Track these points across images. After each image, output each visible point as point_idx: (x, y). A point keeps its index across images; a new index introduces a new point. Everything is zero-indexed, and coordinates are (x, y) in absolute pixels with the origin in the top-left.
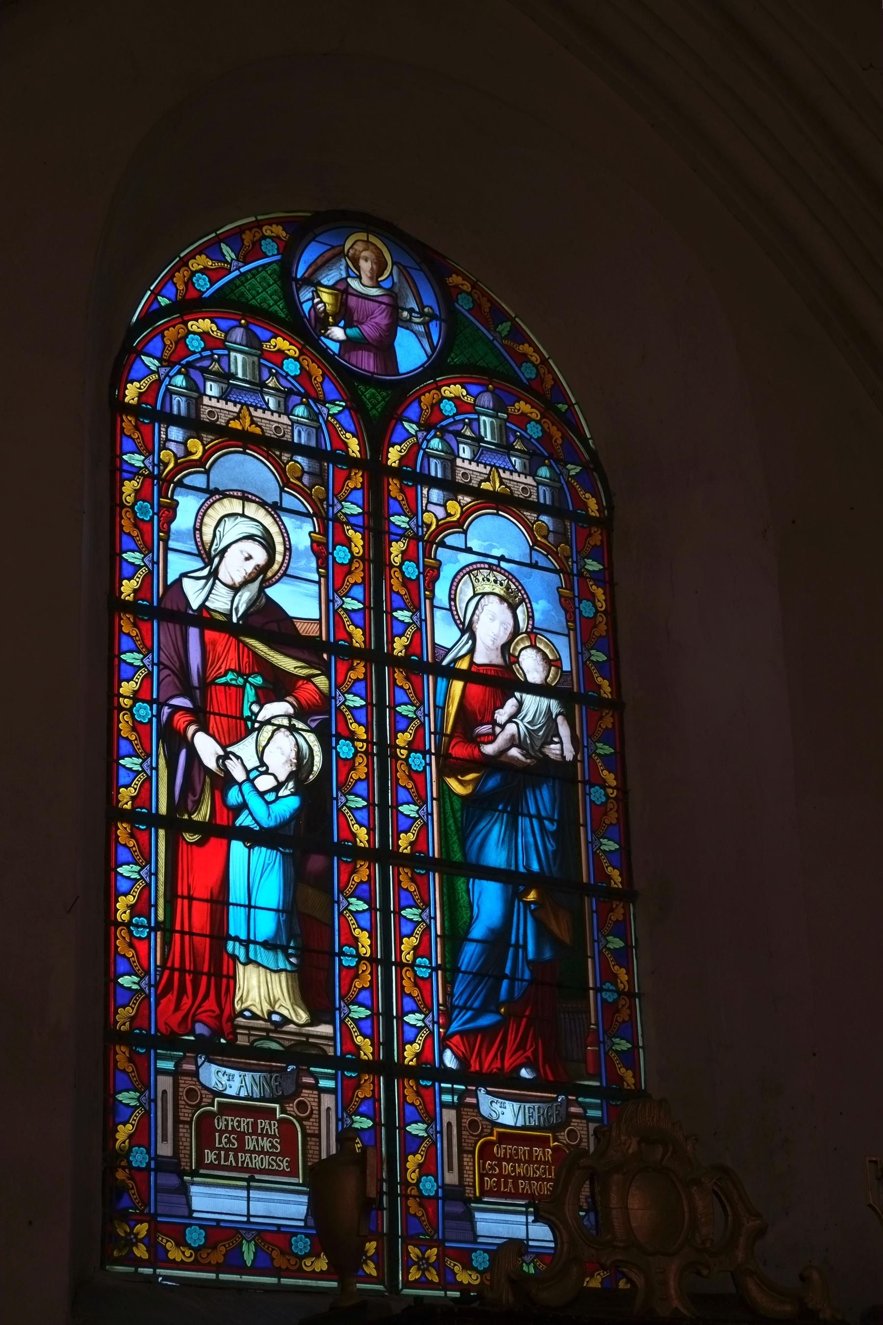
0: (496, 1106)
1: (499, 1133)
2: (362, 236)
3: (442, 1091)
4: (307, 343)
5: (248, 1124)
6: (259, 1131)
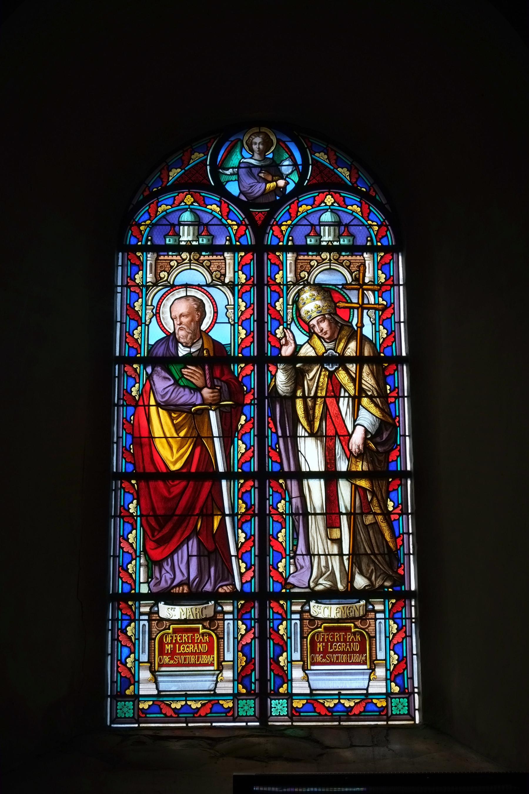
5: (188, 637)
6: (348, 640)
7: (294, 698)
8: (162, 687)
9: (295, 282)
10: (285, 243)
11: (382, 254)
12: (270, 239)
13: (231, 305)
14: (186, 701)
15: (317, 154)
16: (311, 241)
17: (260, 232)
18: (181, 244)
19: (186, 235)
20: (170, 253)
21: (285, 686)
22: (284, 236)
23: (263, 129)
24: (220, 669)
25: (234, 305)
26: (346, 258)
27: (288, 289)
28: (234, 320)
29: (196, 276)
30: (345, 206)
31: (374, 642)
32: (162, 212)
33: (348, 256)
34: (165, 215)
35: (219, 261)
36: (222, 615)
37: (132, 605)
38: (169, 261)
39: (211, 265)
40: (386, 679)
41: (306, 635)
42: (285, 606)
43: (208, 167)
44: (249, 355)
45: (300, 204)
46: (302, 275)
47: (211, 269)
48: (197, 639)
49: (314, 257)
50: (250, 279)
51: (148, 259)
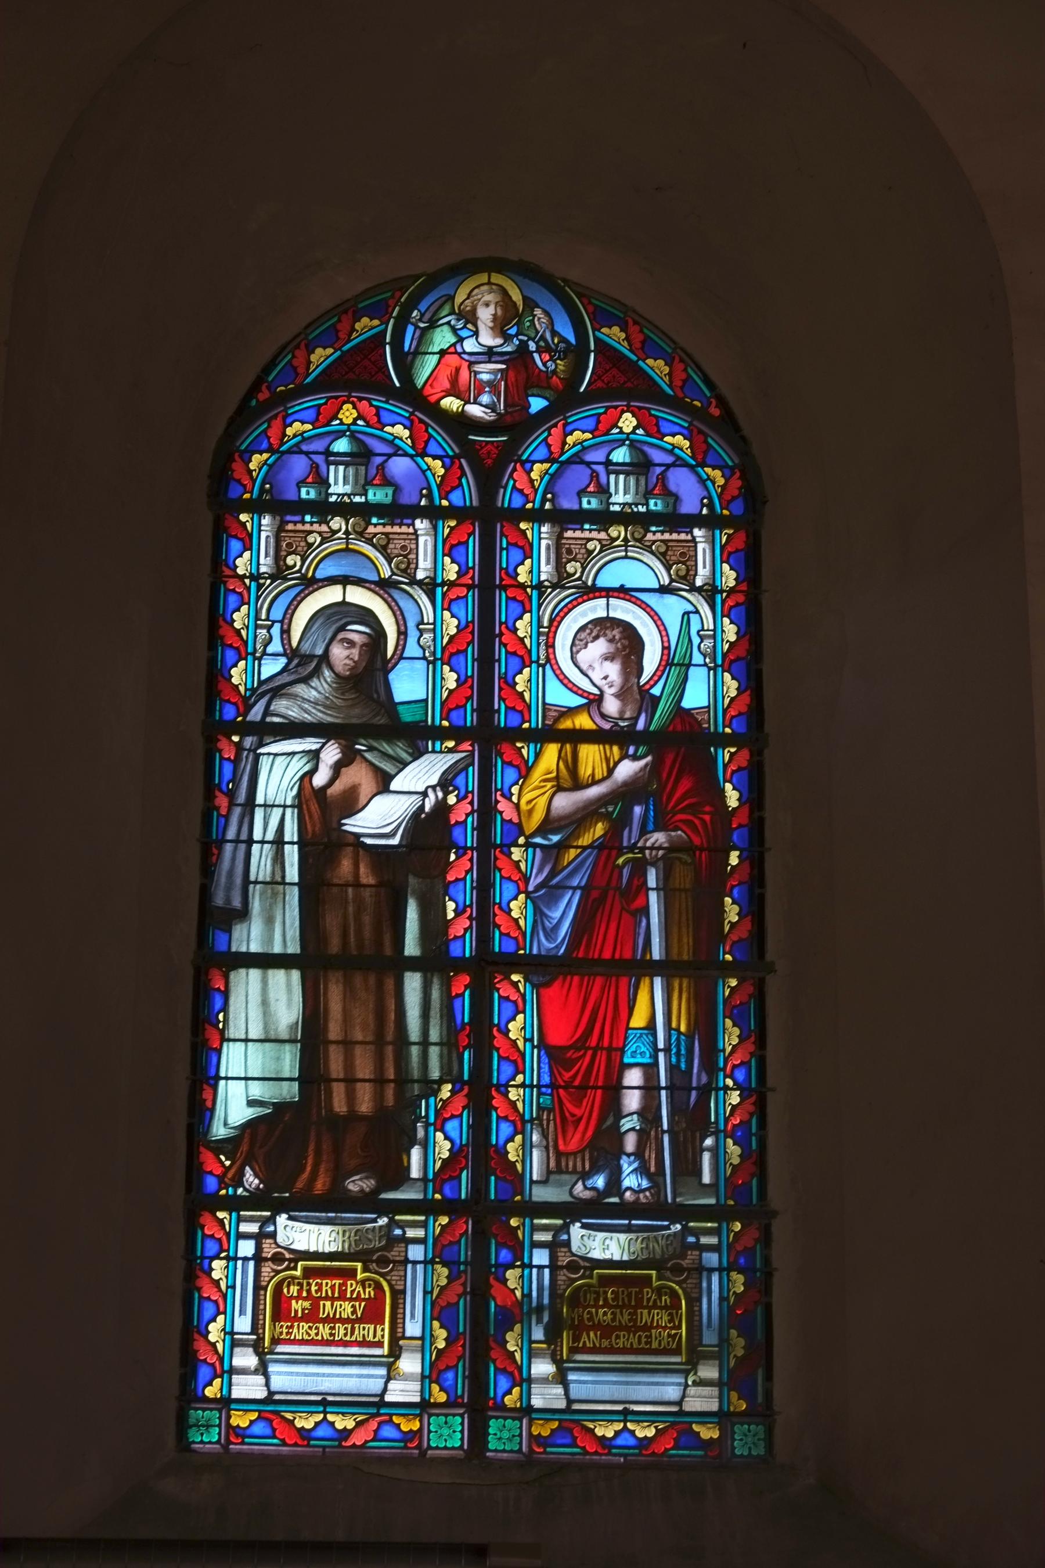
0: (589, 1243)
1: (601, 1277)
2: (484, 278)
3: (534, 1229)
4: (417, 408)
5: (333, 1287)
6: (349, 1296)
7: (233, 1406)
8: (277, 1383)
9: (555, 581)
10: (537, 506)
11: (453, 523)
12: (507, 498)
13: (428, 624)
14: (325, 1413)
15: (604, 330)
16: (590, 503)
17: (489, 483)
18: (612, 508)
19: (340, 484)
20: (587, 526)
21: (217, 1382)
22: (536, 491)
23: (497, 278)
24: (396, 1352)
25: (714, 630)
26: (380, 529)
27: (259, 587)
28: (434, 653)
29: (639, 571)
30: (380, 426)
31: (262, 1297)
32: (574, 445)
33: (384, 525)
34: (579, 452)
35: (405, 536)
36: (697, 1253)
37: (518, 1227)
38: (584, 542)
39: (388, 543)
40: (423, 1377)
41: (264, 1284)
42: (226, 1222)
43: (388, 348)
44: (461, 723)
45: (569, 428)
46: (290, 561)
47: (668, 558)
48: (352, 1292)
49: (594, 534)
50: (467, 573)
51: (543, 536)
